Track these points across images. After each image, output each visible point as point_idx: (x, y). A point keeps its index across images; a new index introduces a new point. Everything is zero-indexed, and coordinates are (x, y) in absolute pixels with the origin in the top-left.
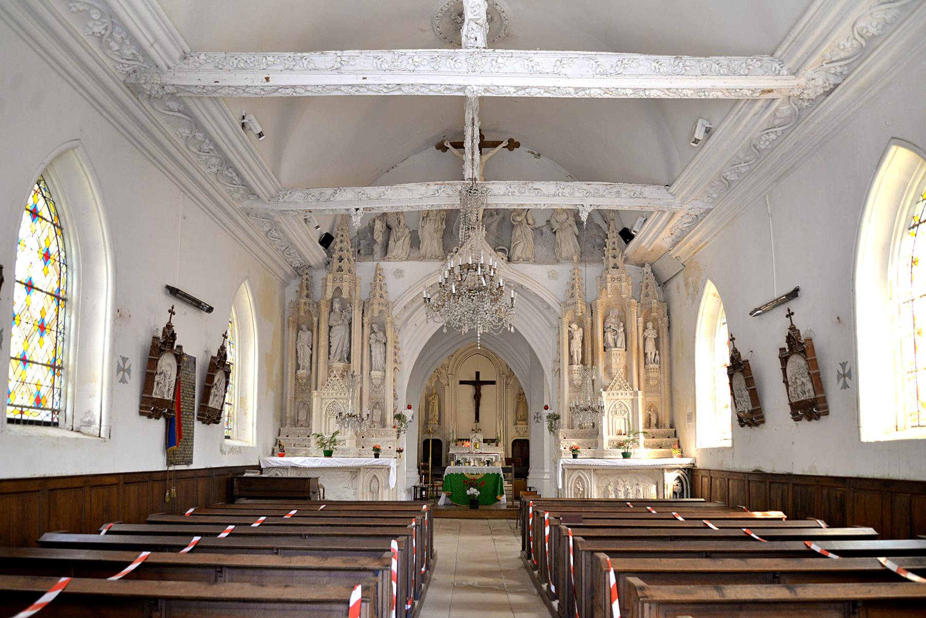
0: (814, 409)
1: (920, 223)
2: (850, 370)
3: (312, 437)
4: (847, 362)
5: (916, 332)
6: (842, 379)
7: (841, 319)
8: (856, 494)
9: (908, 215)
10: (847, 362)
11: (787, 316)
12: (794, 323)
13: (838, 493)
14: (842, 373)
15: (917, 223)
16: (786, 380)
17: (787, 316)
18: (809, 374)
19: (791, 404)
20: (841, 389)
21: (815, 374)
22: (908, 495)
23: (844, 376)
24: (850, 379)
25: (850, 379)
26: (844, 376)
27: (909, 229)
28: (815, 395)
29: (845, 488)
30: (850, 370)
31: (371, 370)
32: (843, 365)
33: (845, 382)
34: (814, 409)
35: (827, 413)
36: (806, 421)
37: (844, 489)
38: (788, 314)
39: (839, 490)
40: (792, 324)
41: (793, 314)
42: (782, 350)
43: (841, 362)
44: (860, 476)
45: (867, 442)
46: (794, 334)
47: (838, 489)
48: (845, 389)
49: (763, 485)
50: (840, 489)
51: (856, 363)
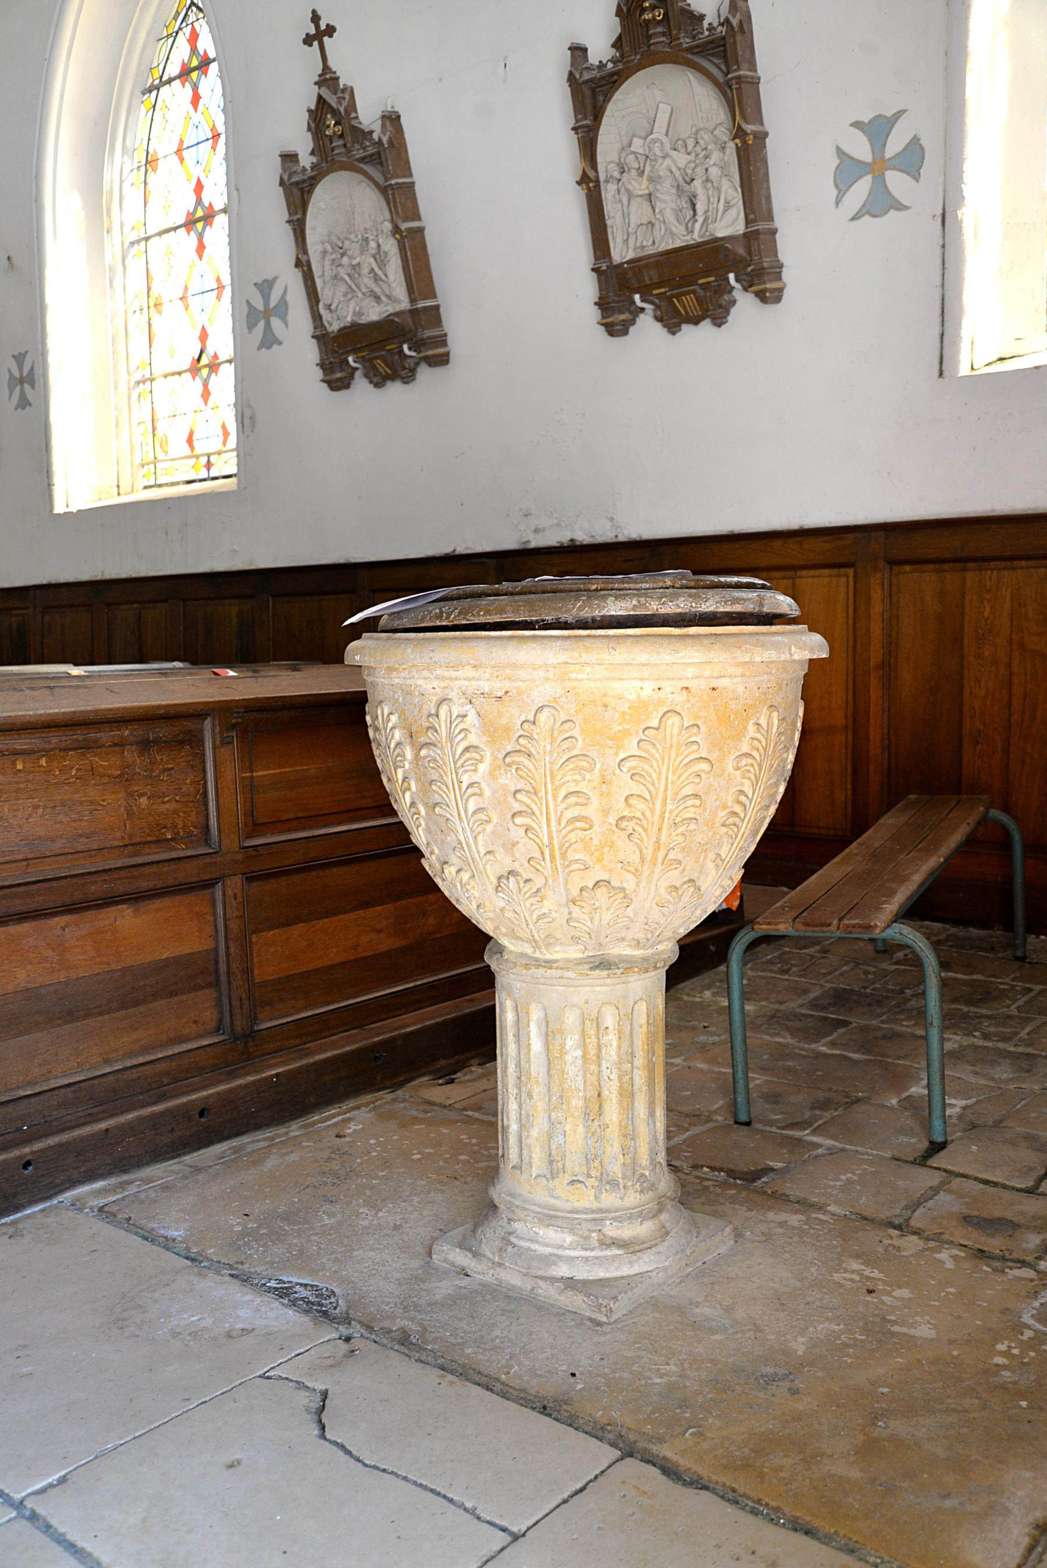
0: (405, 347)
1: (163, 83)
2: (32, 368)
3: (986, 603)
4: (27, 352)
5: (152, 304)
6: (18, 388)
7: (14, 260)
8: (46, 618)
9: (139, 64)
10: (27, 352)
11: (308, 41)
12: (331, 63)
13: (14, 619)
14: (17, 375)
15: (157, 82)
16: (303, 258)
17: (308, 41)
18: (396, 230)
19: (322, 337)
20: (16, 409)
21: (410, 230)
22: (136, 605)
23: (21, 381)
24: (33, 388)
25: (33, 388)
26: (21, 381)
27: (144, 94)
28: (413, 301)
29: (26, 608)
30: (32, 368)
31: (929, 1095)
32: (20, 359)
33: (22, 393)
34: (405, 347)
35: (443, 360)
36: (371, 387)
37: (24, 611)
38: (313, 31)
39: (18, 615)
40: (326, 68)
41: (330, 30)
42: (289, 158)
43: (16, 354)
44: (54, 582)
45: (79, 511)
46: (339, 103)
47: (14, 612)
48: (23, 408)
49: (844, 579)
50: (18, 612)
51: (43, 354)
